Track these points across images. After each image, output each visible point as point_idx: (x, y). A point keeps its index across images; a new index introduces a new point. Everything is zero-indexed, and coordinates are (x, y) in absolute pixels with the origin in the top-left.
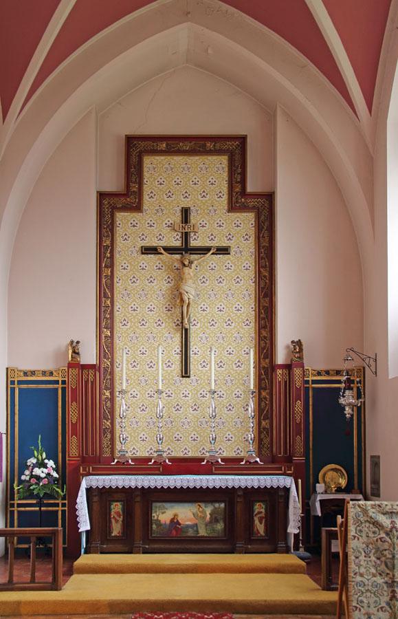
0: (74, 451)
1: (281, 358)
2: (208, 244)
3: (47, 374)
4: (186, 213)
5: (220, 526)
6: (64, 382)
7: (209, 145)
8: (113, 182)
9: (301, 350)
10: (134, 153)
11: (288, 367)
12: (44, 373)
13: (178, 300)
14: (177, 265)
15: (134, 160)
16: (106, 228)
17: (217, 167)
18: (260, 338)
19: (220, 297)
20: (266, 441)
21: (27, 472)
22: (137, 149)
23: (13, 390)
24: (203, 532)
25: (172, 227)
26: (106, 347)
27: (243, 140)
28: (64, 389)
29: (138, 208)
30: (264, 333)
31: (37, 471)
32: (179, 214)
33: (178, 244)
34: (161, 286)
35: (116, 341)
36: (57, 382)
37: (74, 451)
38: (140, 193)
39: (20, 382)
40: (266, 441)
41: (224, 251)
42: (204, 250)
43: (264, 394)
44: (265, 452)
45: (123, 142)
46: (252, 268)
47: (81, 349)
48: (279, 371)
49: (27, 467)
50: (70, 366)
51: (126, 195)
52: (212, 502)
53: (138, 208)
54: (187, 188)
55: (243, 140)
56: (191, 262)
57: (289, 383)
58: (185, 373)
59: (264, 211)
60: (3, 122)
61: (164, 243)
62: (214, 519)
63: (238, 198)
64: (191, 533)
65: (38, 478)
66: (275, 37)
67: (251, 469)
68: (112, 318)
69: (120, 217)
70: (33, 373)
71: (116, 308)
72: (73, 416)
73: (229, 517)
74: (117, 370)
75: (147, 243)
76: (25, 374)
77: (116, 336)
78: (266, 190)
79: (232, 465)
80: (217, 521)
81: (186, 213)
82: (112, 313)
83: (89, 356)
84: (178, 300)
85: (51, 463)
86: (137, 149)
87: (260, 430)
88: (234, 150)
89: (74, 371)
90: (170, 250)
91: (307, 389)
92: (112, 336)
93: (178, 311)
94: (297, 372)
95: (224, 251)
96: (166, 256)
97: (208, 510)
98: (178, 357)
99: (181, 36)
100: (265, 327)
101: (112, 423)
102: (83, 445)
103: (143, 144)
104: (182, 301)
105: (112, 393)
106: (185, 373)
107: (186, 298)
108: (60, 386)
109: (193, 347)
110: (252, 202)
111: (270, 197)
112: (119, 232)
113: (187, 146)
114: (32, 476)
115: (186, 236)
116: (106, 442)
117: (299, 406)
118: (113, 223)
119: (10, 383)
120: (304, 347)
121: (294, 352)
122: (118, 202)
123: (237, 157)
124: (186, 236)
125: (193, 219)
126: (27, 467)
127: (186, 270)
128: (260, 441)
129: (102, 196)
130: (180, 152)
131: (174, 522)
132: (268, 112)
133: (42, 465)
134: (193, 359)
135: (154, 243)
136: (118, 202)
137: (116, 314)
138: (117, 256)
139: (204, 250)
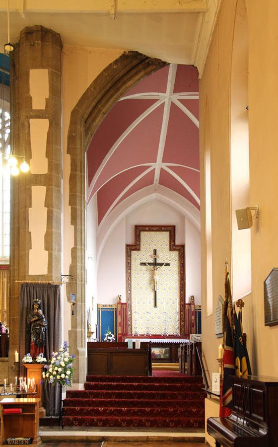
0: (120, 331)
1: (187, 301)
2: (163, 262)
3: (40, 278)
4: (155, 251)
5: (167, 355)
6: (116, 309)
7: (163, 228)
8: (131, 241)
9: (194, 299)
10: (138, 231)
11: (189, 304)
12: (109, 305)
13: (153, 281)
14: (152, 269)
15: (138, 233)
16: (129, 256)
17: (165, 236)
18: (181, 294)
19: (168, 278)
20: (183, 329)
21: (106, 338)
22: (139, 229)
23: (99, 311)
24: (162, 357)
25: (150, 256)
26: (129, 297)
27: (174, 227)
28: (116, 311)
29: (139, 249)
30: (182, 293)
31: (109, 338)
32: (153, 252)
33: (153, 262)
34: (147, 276)
35: (132, 294)
36: (114, 309)
37: (120, 331)
38: (139, 245)
39: (101, 309)
40: (183, 329)
41: (168, 264)
42: (162, 264)
43: (182, 313)
44: (182, 332)
45: (134, 227)
46: (178, 270)
47: (121, 298)
48: (187, 306)
49: (106, 336)
50: (118, 303)
51: (135, 246)
52: (165, 347)
53: (139, 249)
54: (157, 242)
55: (174, 227)
56: (157, 269)
57: (189, 310)
58: (155, 306)
59: (181, 250)
60: (99, 224)
61: (148, 262)
62: (166, 353)
63: (173, 247)
64: (158, 357)
65: (109, 340)
66: (184, 198)
67: (177, 337)
68: (131, 287)
69: (133, 253)
70: (106, 305)
71: (132, 284)
72: (119, 320)
73: (170, 352)
74: (133, 305)
75: (142, 262)
76: (103, 306)
77: (132, 293)
78: (183, 244)
79: (171, 337)
80: (166, 353)
81: (155, 251)
82: (131, 285)
83: (124, 301)
84: (153, 281)
85: (113, 335)
86: (139, 229)
87: (181, 326)
88: (171, 230)
89: (120, 305)
90: (150, 264)
91: (196, 312)
92: (131, 293)
93: (153, 284)
94: (192, 306)
95: (168, 264)
96: (148, 266)
97: (164, 350)
98: (153, 300)
99: (154, 196)
100: (182, 291)
101: (131, 323)
102: (122, 330)
103: (141, 228)
104: (154, 282)
105: (131, 313)
106: (155, 306)
107: (155, 281)
108: (115, 310)
109: (158, 297)
110: (177, 248)
111: (183, 246)
112: (133, 257)
113: (155, 229)
114: (107, 339)
115: (155, 259)
116: (129, 329)
117: (193, 318)
118: (131, 255)
119: (98, 309)
120: (195, 298)
121: (191, 299)
122: (133, 247)
123: (172, 233)
124: (155, 259)
125: (158, 253)
126: (106, 336)
127: (156, 271)
128: (181, 329)
129: (127, 246)
130: (153, 231)
131: (111, 410)
132: (183, 217)
133: (110, 336)
134: (157, 299)
135: (145, 262)
136: (133, 247)
137: (132, 286)
138: (132, 266)
139: (162, 264)
